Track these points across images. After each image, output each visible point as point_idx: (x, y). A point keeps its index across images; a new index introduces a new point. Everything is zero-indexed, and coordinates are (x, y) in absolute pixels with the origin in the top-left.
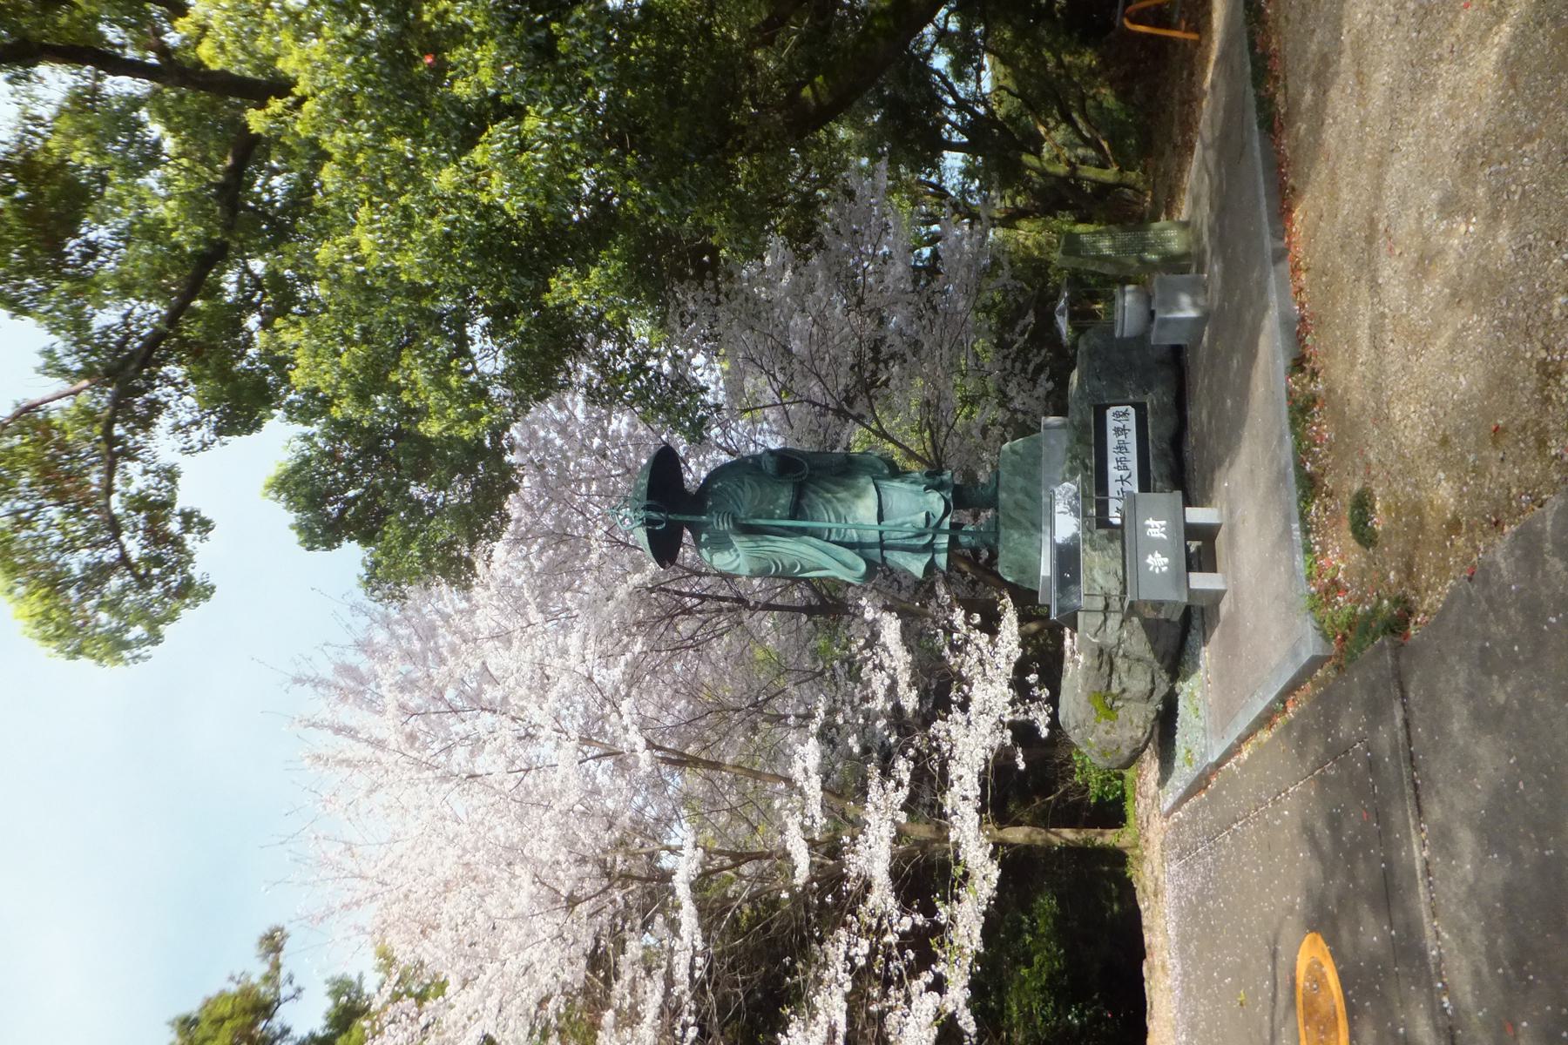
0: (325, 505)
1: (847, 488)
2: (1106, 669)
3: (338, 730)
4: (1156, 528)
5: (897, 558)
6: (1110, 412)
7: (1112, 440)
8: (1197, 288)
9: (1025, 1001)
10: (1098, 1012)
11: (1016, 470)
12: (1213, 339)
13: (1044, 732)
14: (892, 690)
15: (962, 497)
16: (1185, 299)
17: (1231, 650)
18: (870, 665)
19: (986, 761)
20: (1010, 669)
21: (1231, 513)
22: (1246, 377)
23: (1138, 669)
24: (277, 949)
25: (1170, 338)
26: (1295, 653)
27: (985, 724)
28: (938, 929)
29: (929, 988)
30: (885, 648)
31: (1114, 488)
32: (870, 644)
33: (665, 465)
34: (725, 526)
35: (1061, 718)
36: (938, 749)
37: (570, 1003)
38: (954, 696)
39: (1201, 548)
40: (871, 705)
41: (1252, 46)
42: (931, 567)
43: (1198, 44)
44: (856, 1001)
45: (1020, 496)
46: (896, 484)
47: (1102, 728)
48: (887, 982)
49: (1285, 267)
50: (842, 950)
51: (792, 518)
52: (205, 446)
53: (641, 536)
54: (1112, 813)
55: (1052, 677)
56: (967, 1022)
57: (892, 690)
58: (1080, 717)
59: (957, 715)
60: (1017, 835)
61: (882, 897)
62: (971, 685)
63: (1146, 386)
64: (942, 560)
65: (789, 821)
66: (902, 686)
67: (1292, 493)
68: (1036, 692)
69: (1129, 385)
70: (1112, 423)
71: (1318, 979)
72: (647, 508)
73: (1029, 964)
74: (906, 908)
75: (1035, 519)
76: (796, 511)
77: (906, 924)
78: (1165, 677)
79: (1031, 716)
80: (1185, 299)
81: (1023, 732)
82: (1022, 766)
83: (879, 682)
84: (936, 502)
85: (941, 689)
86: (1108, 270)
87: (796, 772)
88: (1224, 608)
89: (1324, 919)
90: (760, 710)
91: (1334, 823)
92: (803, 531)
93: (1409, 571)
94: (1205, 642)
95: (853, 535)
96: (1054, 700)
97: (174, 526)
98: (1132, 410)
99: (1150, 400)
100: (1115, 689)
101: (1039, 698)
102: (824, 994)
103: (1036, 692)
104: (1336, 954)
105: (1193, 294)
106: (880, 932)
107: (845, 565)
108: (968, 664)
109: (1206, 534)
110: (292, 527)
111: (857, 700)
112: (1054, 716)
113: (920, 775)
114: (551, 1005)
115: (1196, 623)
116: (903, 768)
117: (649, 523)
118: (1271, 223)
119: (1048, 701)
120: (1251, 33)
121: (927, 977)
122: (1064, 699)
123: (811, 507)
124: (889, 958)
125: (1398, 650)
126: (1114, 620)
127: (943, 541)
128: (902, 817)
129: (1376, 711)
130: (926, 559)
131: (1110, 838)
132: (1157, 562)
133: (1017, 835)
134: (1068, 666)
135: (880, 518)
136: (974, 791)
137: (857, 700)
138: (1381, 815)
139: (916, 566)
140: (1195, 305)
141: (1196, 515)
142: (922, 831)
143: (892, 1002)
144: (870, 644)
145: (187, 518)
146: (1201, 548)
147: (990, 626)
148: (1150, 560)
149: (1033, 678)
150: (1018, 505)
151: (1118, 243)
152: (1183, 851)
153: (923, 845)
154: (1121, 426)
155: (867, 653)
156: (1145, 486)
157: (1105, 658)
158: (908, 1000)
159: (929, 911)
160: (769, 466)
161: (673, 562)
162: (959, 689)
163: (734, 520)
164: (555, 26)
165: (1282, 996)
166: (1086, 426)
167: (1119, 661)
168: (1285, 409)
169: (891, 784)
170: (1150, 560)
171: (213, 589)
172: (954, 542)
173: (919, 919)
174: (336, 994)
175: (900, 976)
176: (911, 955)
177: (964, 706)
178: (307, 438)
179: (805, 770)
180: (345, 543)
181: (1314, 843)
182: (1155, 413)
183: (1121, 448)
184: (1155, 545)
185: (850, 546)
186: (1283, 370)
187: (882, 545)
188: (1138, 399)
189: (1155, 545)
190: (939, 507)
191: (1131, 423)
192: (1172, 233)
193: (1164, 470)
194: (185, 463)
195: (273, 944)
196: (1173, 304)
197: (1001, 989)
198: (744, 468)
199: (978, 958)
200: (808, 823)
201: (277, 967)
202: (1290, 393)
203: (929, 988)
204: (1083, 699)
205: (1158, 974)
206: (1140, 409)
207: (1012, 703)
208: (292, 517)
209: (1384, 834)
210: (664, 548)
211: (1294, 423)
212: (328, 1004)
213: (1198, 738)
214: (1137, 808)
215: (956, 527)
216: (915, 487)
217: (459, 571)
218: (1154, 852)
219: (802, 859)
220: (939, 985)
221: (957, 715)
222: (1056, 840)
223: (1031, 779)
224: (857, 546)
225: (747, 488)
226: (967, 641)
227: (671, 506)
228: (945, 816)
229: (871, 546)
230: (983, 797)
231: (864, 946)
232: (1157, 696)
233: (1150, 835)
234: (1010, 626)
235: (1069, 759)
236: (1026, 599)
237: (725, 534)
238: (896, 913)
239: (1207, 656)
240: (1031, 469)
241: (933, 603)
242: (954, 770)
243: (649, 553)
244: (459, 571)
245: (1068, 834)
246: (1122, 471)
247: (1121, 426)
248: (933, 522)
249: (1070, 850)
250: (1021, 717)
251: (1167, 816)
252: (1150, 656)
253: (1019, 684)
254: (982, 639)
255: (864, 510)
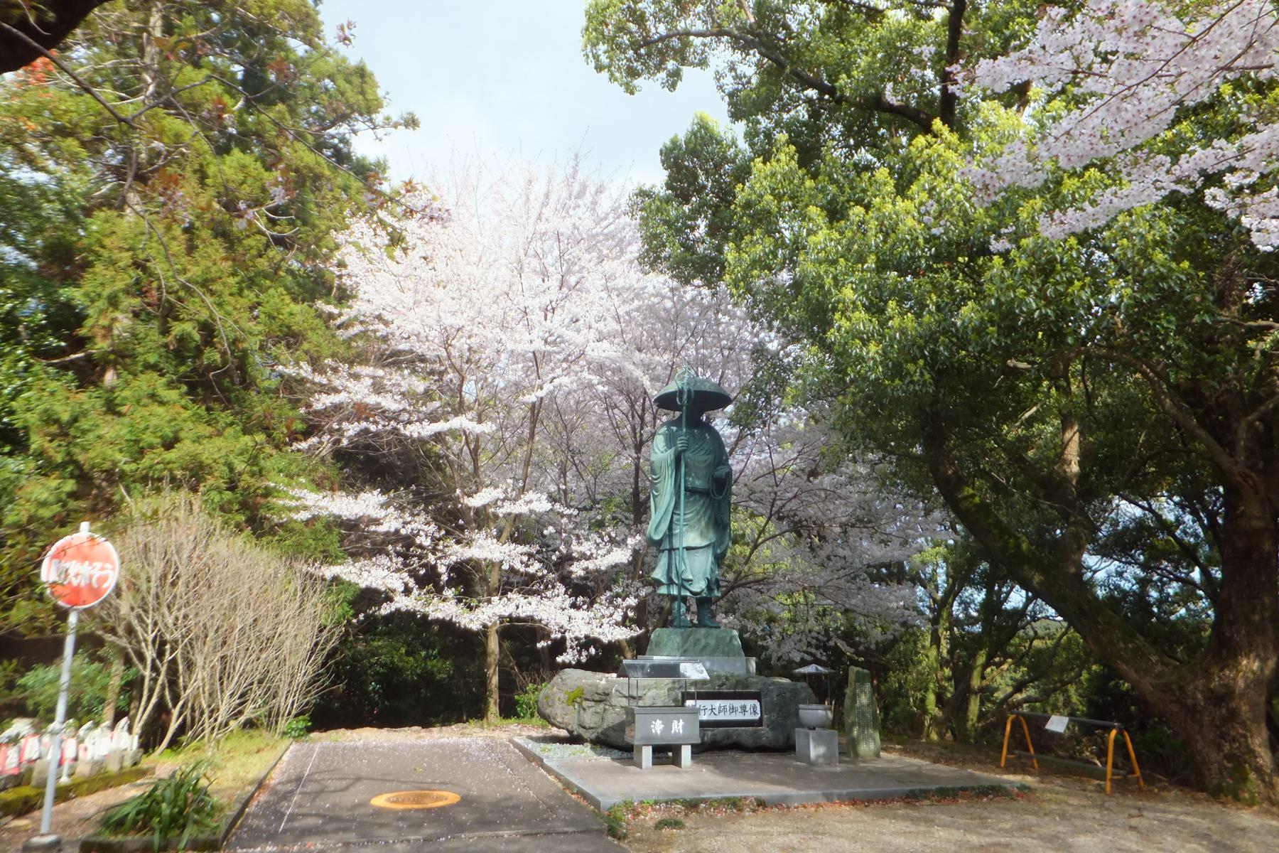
0: (691, 162)
1: (707, 524)
2: (597, 698)
3: (547, 196)
4: (678, 726)
5: (664, 560)
6: (756, 702)
7: (738, 703)
8: (828, 758)
9: (385, 650)
10: (377, 704)
11: (720, 640)
12: (796, 767)
13: (559, 659)
14: (584, 557)
15: (704, 602)
16: (822, 750)
17: (607, 770)
18: (599, 540)
19: (540, 621)
20: (596, 635)
21: (686, 772)
22: (762, 781)
23: (597, 719)
24: (407, 125)
25: (799, 742)
26: (602, 795)
27: (562, 620)
28: (439, 590)
29: (406, 585)
30: (609, 552)
31: (707, 703)
32: (612, 540)
33: (717, 400)
34: (680, 444)
35: (567, 670)
36: (546, 588)
37: (385, 339)
38: (580, 599)
39: (666, 753)
40: (574, 542)
41: (964, 789)
42: (658, 583)
43: (998, 766)
44: (395, 537)
45: (703, 642)
46: (711, 559)
47: (562, 695)
48: (406, 556)
49: (822, 800)
50: (423, 528)
51: (686, 489)
52: (721, 88)
53: (672, 387)
54: (509, 710)
55: (593, 665)
56: (386, 609)
57: (584, 557)
58: (568, 681)
59: (569, 601)
60: (493, 644)
61: (457, 553)
62: (588, 609)
63: (773, 726)
64: (663, 590)
65: (499, 490)
66: (584, 564)
67: (689, 797)
68: (584, 653)
69: (774, 716)
70: (749, 703)
71: (439, 799)
72: (689, 391)
73: (408, 654)
74: (451, 568)
75: (692, 651)
76: (691, 491)
77: (442, 569)
78: (593, 736)
79: (569, 650)
80: (822, 750)
81: (559, 646)
82: (539, 645)
83: (586, 547)
84: (699, 586)
85: (585, 590)
86: (847, 701)
87: (530, 495)
88: (632, 768)
89: (466, 801)
90: (570, 458)
91: (516, 807)
92: (678, 497)
93: (640, 840)
94: (613, 759)
95: (676, 531)
96: (579, 665)
97: (671, 64)
98: (757, 717)
99: (764, 730)
100: (585, 704)
101: (580, 655)
102: (396, 514)
103: (584, 653)
104: (452, 806)
105: (824, 756)
106: (434, 551)
107: (658, 525)
108: (601, 608)
109: (676, 761)
110: (676, 136)
111: (577, 532)
112: (569, 666)
113: (532, 578)
114: (381, 326)
115: (625, 755)
116: (535, 567)
117: (681, 392)
118: (848, 794)
119: (579, 661)
120: (973, 789)
121: (412, 583)
122: (580, 672)
123: (695, 501)
124: (420, 557)
125: (600, 832)
126: (624, 702)
127: (674, 591)
128: (505, 567)
129: (571, 823)
130: (664, 580)
131: (493, 709)
132: (657, 727)
133: (493, 644)
134: (600, 675)
135: (688, 549)
136: (522, 613)
137: (577, 532)
138: (521, 822)
139: (659, 574)
140: (818, 757)
141: (686, 752)
142: (494, 579)
143: (394, 560)
144: (612, 540)
145: (675, 75)
146: (666, 753)
147: (625, 622)
148: (659, 722)
149: (592, 651)
150: (697, 641)
151: (865, 709)
152: (491, 747)
153: (484, 579)
154: (747, 710)
155: (606, 539)
156: (704, 725)
157: (603, 697)
158: (397, 570)
159: (450, 583)
160: (721, 472)
161: (659, 406)
162: (584, 603)
163: (684, 451)
164: (921, 362)
165: (425, 786)
166: (747, 686)
167: (602, 706)
168: (739, 795)
169: (525, 559)
170: (659, 722)
171: (632, 93)
172: (673, 598)
173: (445, 578)
174: (378, 164)
175: (408, 565)
176: (422, 572)
177: (574, 606)
178: (734, 143)
179: (531, 502)
180: (666, 173)
181: (505, 799)
182: (755, 732)
183: (733, 709)
184: (668, 726)
185: (670, 528)
186: (759, 794)
187: (671, 550)
188: (765, 722)
189: (668, 726)
190: (696, 588)
191: (749, 716)
192: (872, 746)
193: (719, 738)
194: (709, 73)
195: (412, 122)
196: (818, 744)
197: (388, 634)
198: (719, 454)
199: (425, 616)
200: (499, 503)
201: (395, 126)
202: (746, 798)
203: (406, 585)
204: (578, 683)
205: (415, 735)
206: (759, 723)
207: (577, 639)
208: (682, 137)
209: (510, 823)
210: (666, 402)
211: (728, 799)
212: (371, 158)
213: (556, 755)
214: (513, 725)
215: (684, 599)
216: (708, 571)
217: (651, 259)
218: (486, 733)
219: (476, 501)
220: (407, 591)
221: (569, 601)
222: (491, 671)
223: (530, 650)
224: (670, 533)
225: (706, 457)
226: (616, 607)
227: (694, 407)
228: (504, 594)
229: (671, 542)
230: (518, 619)
231: (427, 542)
232: (582, 731)
233: (497, 732)
234: (622, 634)
235: (543, 680)
236: (640, 645)
237: (675, 445)
238: (446, 562)
239: (606, 760)
240: (721, 649)
241: (640, 584)
242: (534, 599)
243: (663, 392)
244: (651, 259)
245: (495, 680)
246: (713, 710)
247: (747, 710)
248: (686, 584)
249: (483, 681)
250: (568, 643)
251: (511, 741)
252: (605, 726)
253: (589, 642)
254: (618, 616)
255: (692, 538)
